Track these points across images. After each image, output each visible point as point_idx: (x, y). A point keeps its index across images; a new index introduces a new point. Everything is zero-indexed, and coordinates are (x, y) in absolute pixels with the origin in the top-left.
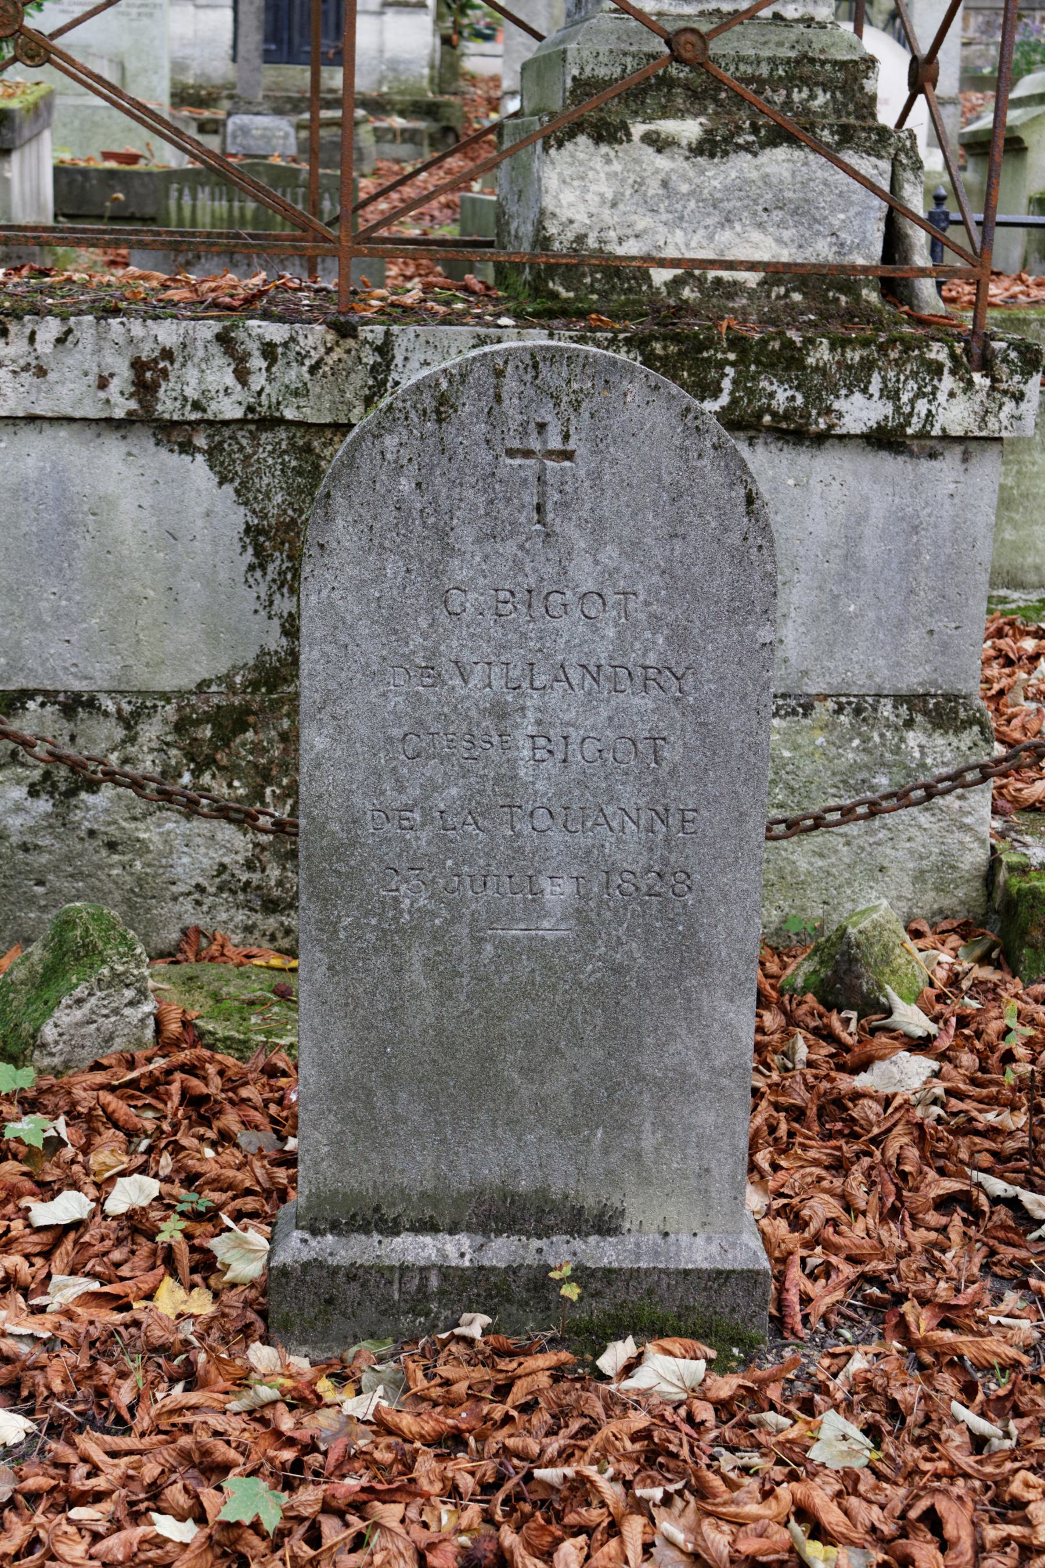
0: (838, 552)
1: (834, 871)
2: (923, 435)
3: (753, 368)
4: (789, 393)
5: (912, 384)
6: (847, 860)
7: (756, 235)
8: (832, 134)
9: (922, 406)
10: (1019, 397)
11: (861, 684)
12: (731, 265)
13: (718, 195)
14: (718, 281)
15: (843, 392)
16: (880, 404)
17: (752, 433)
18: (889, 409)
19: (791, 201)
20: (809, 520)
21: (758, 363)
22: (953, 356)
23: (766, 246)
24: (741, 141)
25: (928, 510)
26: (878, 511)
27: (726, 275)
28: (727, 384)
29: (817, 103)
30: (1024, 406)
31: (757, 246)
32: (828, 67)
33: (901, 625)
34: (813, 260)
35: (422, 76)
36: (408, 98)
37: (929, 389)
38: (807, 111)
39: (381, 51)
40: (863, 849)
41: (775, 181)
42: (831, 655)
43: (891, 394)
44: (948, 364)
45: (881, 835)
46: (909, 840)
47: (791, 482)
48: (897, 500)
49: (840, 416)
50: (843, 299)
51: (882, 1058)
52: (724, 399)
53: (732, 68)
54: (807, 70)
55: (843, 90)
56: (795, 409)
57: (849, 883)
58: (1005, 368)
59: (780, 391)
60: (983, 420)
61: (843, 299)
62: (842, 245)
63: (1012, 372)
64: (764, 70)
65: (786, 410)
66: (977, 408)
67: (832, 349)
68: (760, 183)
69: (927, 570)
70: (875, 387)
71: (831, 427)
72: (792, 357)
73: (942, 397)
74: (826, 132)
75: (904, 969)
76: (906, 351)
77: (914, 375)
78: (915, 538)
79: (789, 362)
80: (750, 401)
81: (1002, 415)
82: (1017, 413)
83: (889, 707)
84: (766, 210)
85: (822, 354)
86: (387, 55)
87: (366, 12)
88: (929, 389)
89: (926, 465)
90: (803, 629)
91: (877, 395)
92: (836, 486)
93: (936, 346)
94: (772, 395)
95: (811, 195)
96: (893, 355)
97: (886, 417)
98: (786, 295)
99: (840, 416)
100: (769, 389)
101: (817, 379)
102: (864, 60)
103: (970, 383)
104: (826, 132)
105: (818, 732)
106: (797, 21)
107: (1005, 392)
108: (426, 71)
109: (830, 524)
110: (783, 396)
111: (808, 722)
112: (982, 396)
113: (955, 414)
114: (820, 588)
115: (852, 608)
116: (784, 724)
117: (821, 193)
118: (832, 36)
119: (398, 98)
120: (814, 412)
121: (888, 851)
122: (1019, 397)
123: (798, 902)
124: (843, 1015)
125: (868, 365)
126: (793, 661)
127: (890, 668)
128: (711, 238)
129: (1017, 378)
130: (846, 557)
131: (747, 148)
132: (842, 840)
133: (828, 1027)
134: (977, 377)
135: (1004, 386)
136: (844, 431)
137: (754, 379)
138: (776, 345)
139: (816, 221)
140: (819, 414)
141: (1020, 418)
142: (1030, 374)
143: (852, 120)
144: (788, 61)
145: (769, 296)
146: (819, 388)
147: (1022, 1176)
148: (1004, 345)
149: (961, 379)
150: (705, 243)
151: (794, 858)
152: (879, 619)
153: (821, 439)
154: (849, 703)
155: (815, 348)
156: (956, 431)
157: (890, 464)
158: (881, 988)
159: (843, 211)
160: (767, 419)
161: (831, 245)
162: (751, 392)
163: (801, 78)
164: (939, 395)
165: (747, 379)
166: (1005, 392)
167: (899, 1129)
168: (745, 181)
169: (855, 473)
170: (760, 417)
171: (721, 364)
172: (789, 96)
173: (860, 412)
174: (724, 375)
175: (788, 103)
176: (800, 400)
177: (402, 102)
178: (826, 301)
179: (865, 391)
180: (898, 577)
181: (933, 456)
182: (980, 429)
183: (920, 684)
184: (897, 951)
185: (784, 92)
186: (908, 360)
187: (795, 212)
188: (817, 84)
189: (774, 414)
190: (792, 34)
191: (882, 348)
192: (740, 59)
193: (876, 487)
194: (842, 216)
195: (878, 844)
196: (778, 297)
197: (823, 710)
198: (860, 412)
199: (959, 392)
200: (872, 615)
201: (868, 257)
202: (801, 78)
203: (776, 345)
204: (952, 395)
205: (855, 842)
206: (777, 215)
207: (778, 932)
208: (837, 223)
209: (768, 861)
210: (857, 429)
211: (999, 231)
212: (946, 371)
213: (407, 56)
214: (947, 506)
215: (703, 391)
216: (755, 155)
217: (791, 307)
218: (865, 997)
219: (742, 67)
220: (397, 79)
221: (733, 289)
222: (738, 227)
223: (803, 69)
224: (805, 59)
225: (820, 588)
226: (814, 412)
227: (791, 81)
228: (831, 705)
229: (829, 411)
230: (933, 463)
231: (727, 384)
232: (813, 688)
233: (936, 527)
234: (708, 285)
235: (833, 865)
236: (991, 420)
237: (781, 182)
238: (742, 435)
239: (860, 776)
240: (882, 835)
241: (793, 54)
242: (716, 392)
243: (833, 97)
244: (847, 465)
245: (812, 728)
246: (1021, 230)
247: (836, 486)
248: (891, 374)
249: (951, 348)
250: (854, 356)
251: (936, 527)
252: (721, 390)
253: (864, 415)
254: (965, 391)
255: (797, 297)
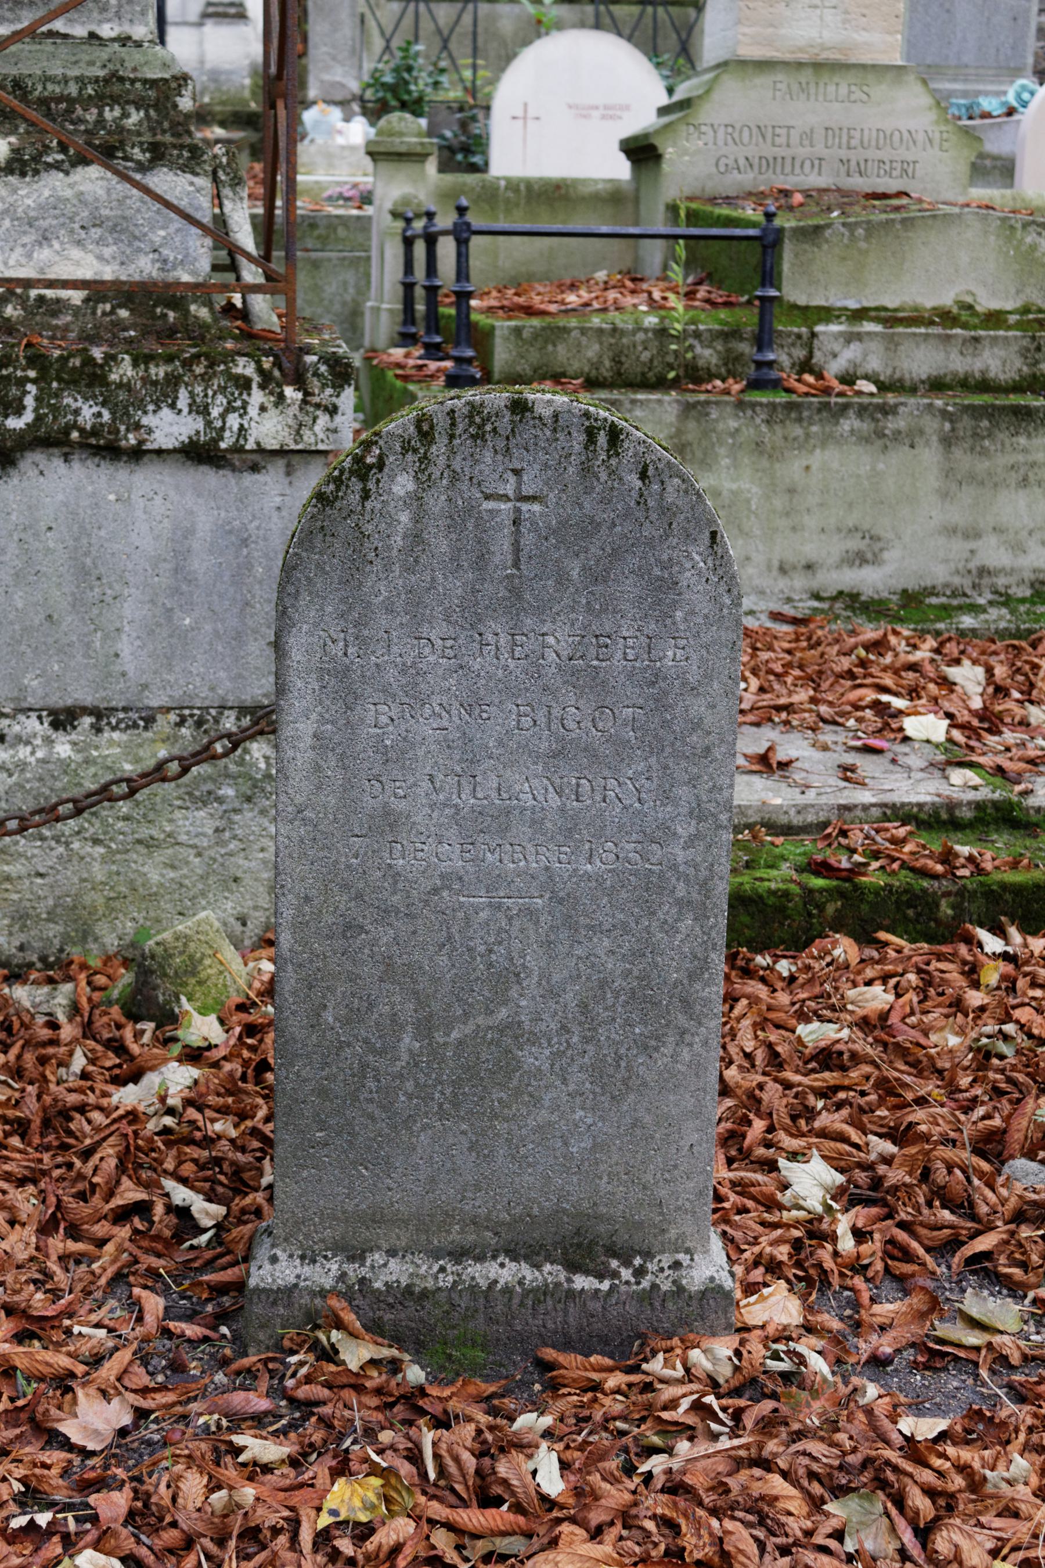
0: (168, 566)
1: (187, 882)
2: (238, 449)
3: (55, 385)
4: (95, 409)
5: (221, 399)
6: (199, 871)
7: (76, 253)
8: (143, 151)
9: (233, 421)
10: (332, 411)
11: (204, 696)
12: (51, 284)
13: (32, 214)
14: (41, 299)
15: (151, 407)
16: (190, 419)
17: (66, 450)
18: (200, 424)
19: (108, 218)
20: (134, 535)
21: (60, 380)
22: (260, 370)
23: (86, 264)
24: (50, 160)
25: (256, 523)
26: (205, 522)
27: (49, 293)
28: (29, 401)
29: (131, 121)
30: (338, 419)
31: (78, 263)
32: (138, 85)
33: (239, 637)
34: (137, 278)
35: (243, 87)
36: (229, 108)
37: (239, 403)
38: (121, 129)
39: (202, 62)
40: (215, 860)
41: (90, 199)
42: (170, 668)
43: (201, 409)
44: (256, 379)
45: (232, 846)
46: (262, 850)
47: (112, 497)
48: (223, 514)
49: (150, 431)
50: (171, 315)
51: (152, 1069)
52: (28, 417)
53: (40, 88)
54: (116, 88)
55: (156, 107)
56: (102, 425)
57: (203, 894)
58: (316, 382)
59: (85, 407)
60: (298, 432)
61: (171, 315)
62: (165, 261)
63: (324, 386)
64: (73, 89)
65: (94, 426)
66: (290, 421)
67: (135, 364)
68: (75, 202)
69: (260, 582)
70: (183, 402)
71: (141, 442)
72: (94, 374)
73: (253, 411)
74: (136, 150)
75: (214, 979)
76: (212, 365)
77: (223, 390)
78: (245, 551)
79: (92, 378)
80: (55, 418)
81: (317, 428)
82: (332, 426)
83: (232, 719)
84: (83, 227)
85: (125, 370)
86: (208, 66)
87: (177, 24)
88: (239, 403)
89: (249, 479)
90: (138, 643)
91: (186, 410)
92: (158, 500)
93: (242, 361)
94: (77, 412)
95: (129, 213)
96: (199, 370)
97: (198, 433)
98: (113, 312)
99: (150, 431)
100: (74, 405)
101: (122, 396)
102: (175, 78)
103: (281, 397)
104: (136, 150)
105: (159, 744)
106: (113, 40)
107: (318, 406)
108: (247, 82)
109: (157, 538)
110: (88, 412)
111: (149, 734)
112: (294, 410)
113: (268, 427)
114: (152, 601)
115: (187, 621)
116: (125, 737)
117: (138, 211)
118: (145, 54)
119: (218, 108)
120: (123, 428)
121: (241, 862)
122: (332, 411)
123: (152, 914)
124: (139, 1026)
125: (173, 382)
126: (131, 674)
127: (231, 679)
128: (29, 256)
129: (329, 391)
130: (176, 570)
131: (57, 166)
132: (192, 852)
133: (121, 1040)
134: (289, 391)
135: (316, 400)
136: (155, 446)
137: (57, 395)
138: (77, 362)
139: (136, 238)
140: (128, 430)
141: (335, 431)
142: (342, 387)
143: (168, 138)
144: (97, 80)
145: (94, 313)
146: (126, 404)
147: (207, 1185)
148: (315, 358)
149: (271, 393)
150: (23, 261)
151: (146, 869)
152: (216, 631)
153: (137, 454)
154: (192, 716)
155: (118, 365)
156: (272, 444)
157: (209, 477)
158: (178, 1000)
159: (163, 228)
160: (75, 435)
161: (153, 261)
162: (55, 409)
163: (111, 97)
164: (249, 409)
165: (50, 397)
166: (318, 406)
167: (112, 1140)
168: (59, 199)
169: (177, 487)
170: (67, 434)
171: (22, 382)
172: (101, 114)
173: (170, 427)
174: (25, 393)
175: (100, 121)
176: (106, 416)
177: (222, 113)
178: (154, 317)
179: (173, 406)
180: (232, 590)
181: (255, 468)
182: (296, 442)
183: (265, 695)
184: (207, 962)
185: (95, 111)
186: (215, 374)
187: (113, 230)
188: (128, 102)
189: (82, 431)
190: (104, 54)
191: (187, 364)
192: (47, 79)
193: (200, 501)
194: (162, 233)
195: (231, 854)
196: (104, 314)
197: (164, 723)
198: (170, 427)
199: (270, 406)
200: (208, 627)
201: (193, 273)
202: (111, 97)
203: (77, 362)
204: (263, 409)
205: (207, 853)
206: (96, 233)
207: (133, 945)
208: (157, 240)
209: (118, 873)
210: (168, 444)
211: (476, 241)
212: (254, 386)
213: (227, 67)
214: (275, 519)
215: (6, 408)
216: (67, 173)
217: (120, 325)
218: (161, 1008)
219: (50, 87)
220: (218, 89)
221: (57, 307)
222: (56, 245)
223: (112, 88)
224: (114, 77)
225: (152, 601)
226: (123, 428)
227: (101, 100)
228: (173, 717)
229: (138, 426)
230: (257, 476)
231: (29, 401)
232: (155, 700)
233: (265, 539)
234: (31, 302)
235: (186, 877)
236: (306, 434)
237: (97, 200)
238: (56, 451)
239: (205, 788)
240: (233, 846)
241: (101, 73)
242: (19, 410)
243: (147, 115)
244: (167, 479)
245: (154, 741)
246: (659, 242)
247: (158, 500)
248: (199, 389)
249: (258, 363)
250: (159, 372)
251: (265, 539)
252: (24, 408)
253: (175, 429)
254: (276, 405)
255: (124, 313)
